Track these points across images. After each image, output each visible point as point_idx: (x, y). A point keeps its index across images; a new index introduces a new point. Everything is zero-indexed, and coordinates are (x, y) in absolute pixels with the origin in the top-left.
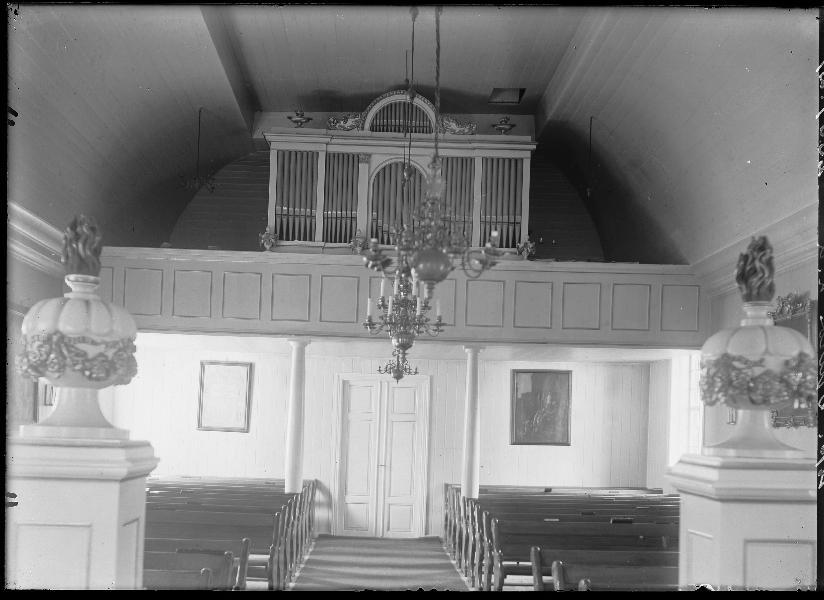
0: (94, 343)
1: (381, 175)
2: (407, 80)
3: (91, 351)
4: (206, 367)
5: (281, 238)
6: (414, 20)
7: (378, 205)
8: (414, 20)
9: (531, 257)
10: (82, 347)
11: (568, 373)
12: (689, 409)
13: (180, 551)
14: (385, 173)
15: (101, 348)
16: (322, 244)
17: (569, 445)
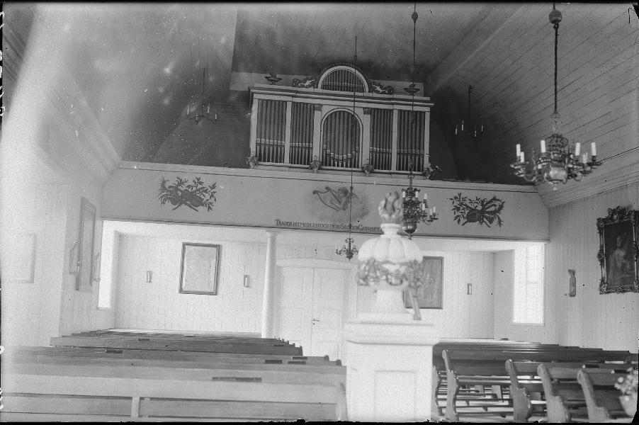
0: (392, 263)
1: (329, 119)
2: (356, 56)
3: (392, 268)
4: (187, 247)
5: (260, 160)
6: (415, 22)
7: (328, 142)
8: (415, 22)
9: (432, 178)
10: (387, 266)
11: (441, 259)
12: (527, 283)
13: (108, 352)
14: (330, 120)
15: (397, 267)
16: (290, 165)
17: (440, 308)
